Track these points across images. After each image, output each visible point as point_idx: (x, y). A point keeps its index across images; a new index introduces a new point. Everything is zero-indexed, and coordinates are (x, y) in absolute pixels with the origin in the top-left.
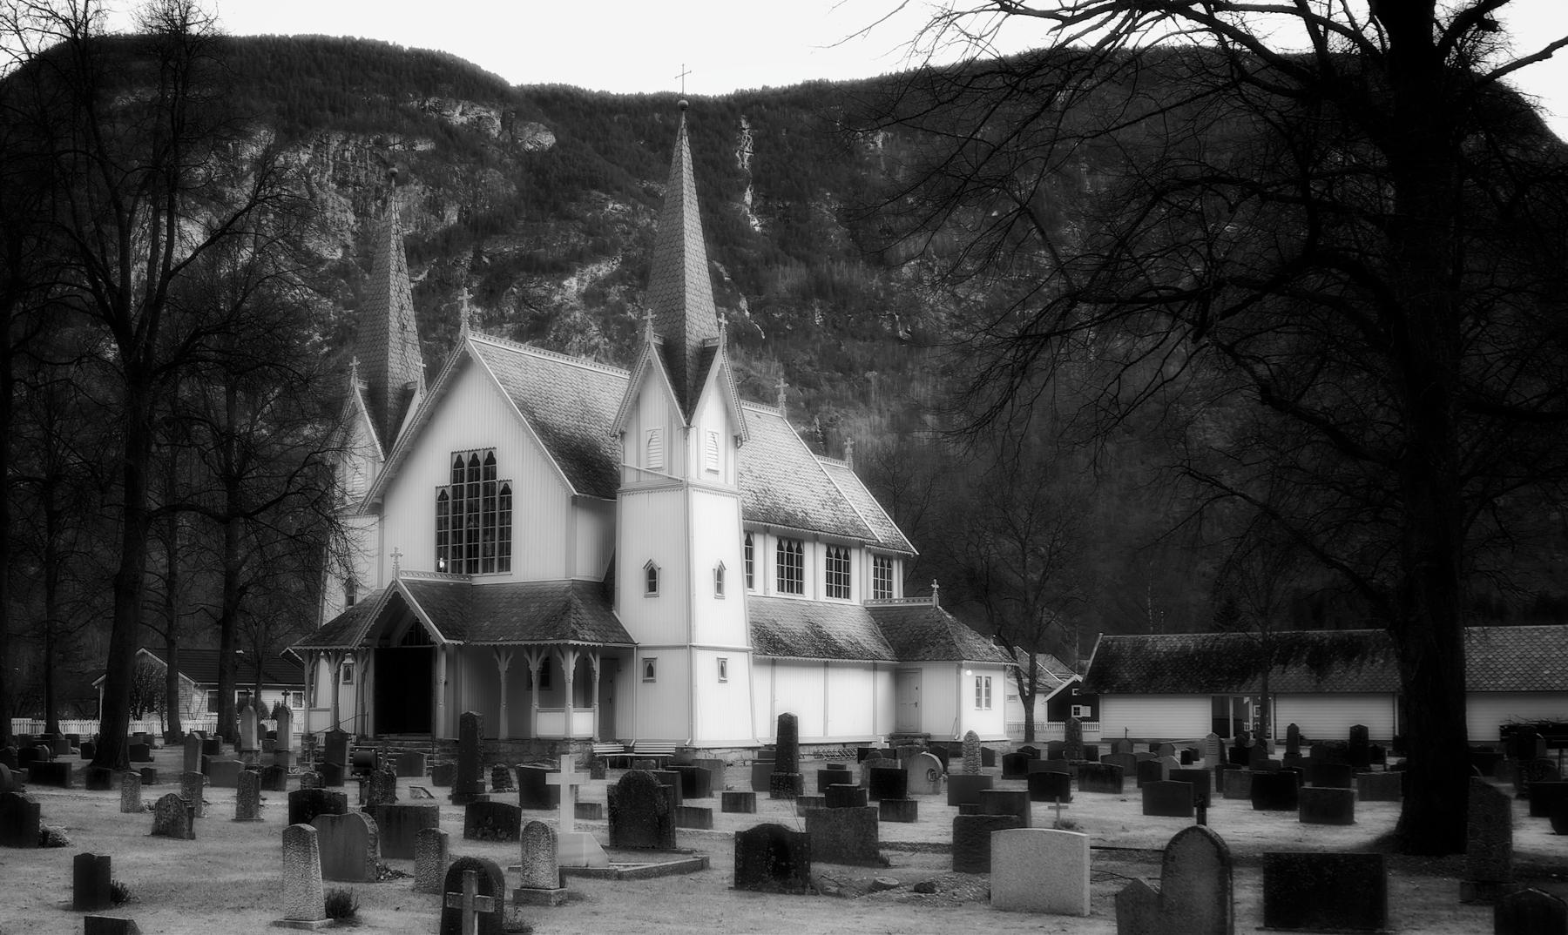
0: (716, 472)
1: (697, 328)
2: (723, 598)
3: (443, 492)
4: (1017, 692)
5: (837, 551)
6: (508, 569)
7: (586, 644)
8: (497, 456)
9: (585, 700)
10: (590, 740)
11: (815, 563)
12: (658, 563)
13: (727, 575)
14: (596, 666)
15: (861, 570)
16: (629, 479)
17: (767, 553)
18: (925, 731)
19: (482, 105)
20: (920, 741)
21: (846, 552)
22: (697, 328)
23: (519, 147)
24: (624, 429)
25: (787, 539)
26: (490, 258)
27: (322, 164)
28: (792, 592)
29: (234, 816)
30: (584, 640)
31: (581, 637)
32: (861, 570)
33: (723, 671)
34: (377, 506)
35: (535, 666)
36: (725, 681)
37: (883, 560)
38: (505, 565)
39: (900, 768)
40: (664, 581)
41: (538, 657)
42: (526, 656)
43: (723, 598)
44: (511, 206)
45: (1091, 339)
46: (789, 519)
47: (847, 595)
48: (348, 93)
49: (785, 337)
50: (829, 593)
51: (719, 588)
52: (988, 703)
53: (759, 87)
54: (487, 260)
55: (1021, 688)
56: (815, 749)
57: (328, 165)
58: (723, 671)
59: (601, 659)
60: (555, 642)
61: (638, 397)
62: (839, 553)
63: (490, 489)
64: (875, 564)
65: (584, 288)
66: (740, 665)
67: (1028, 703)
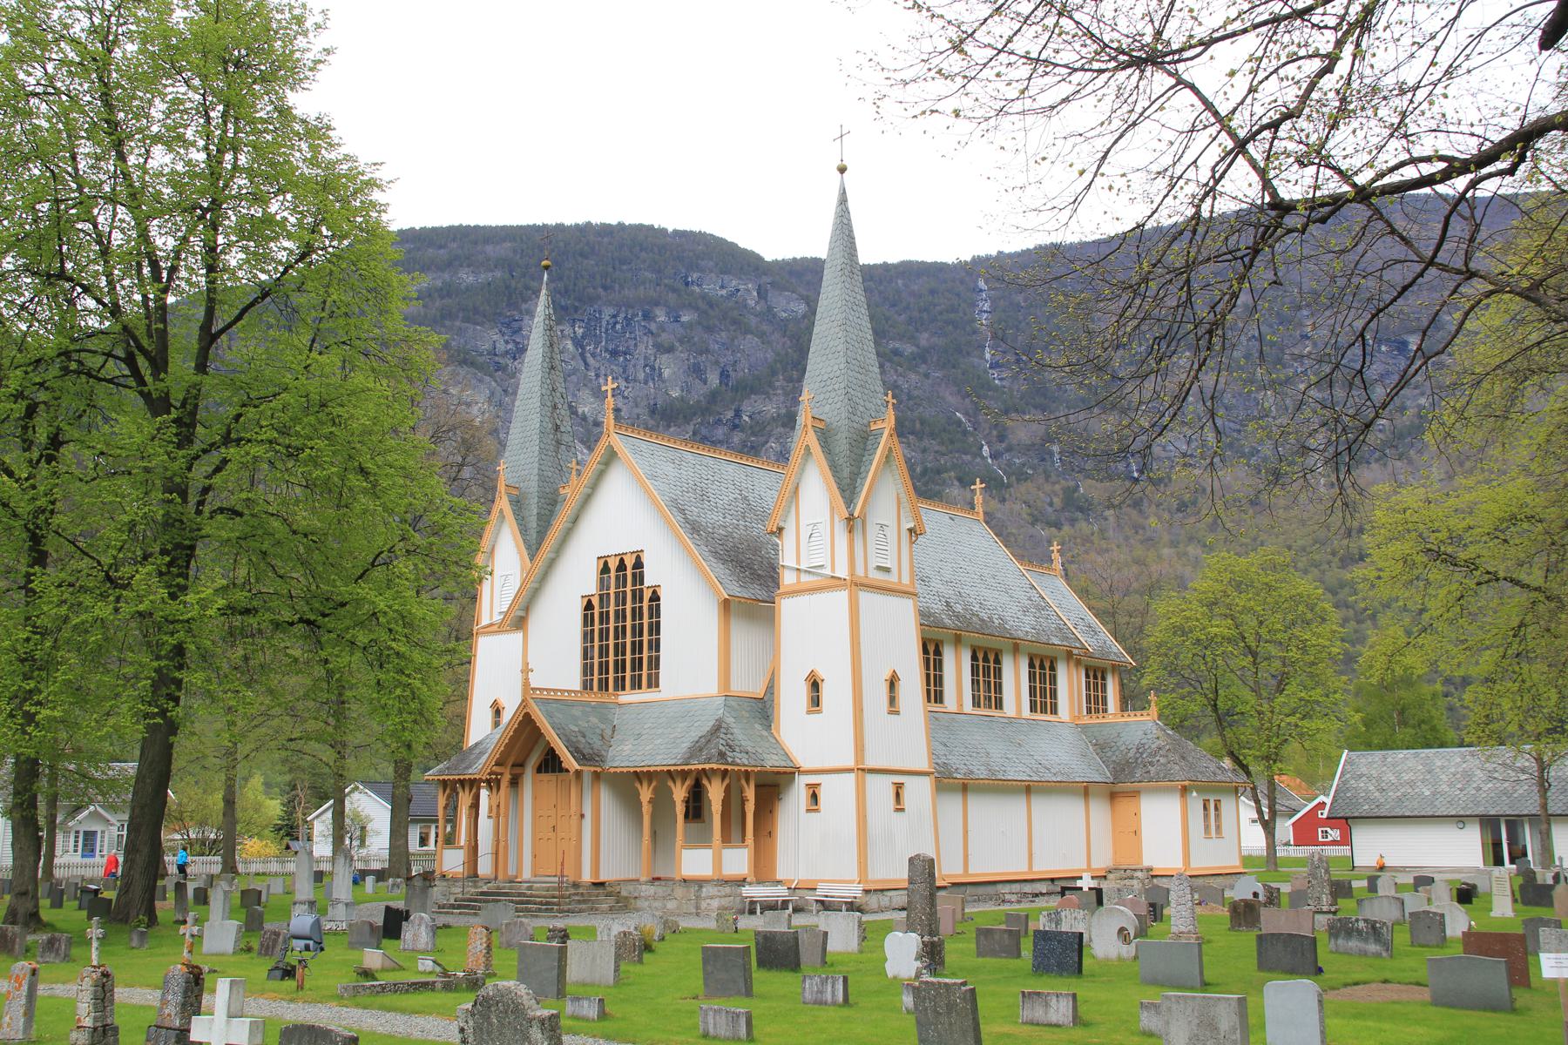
0: (887, 570)
1: (861, 409)
3: (589, 602)
4: (1256, 816)
5: (1042, 662)
6: (657, 686)
7: (736, 768)
8: (645, 560)
10: (742, 882)
11: (1015, 678)
12: (822, 673)
14: (750, 793)
15: (1069, 684)
16: (788, 579)
17: (957, 669)
18: (1146, 863)
19: (740, 279)
20: (1139, 874)
21: (1052, 662)
22: (861, 409)
23: (774, 316)
24: (782, 524)
26: (750, 417)
27: (595, 335)
28: (990, 707)
30: (733, 763)
31: (730, 760)
32: (1069, 684)
34: (518, 620)
35: (680, 793)
36: (817, 811)
37: (1096, 674)
38: (654, 682)
40: (803, 691)
42: (743, 782)
43: (897, 713)
45: (1348, 23)
46: (984, 627)
47: (1054, 711)
48: (617, 273)
49: (1026, 480)
50: (1033, 709)
51: (892, 700)
54: (747, 419)
55: (1260, 812)
56: (1015, 888)
57: (601, 337)
59: (757, 786)
60: (700, 767)
61: (797, 488)
62: (1042, 668)
63: (638, 596)
64: (1087, 676)
66: (919, 791)
67: (1268, 827)
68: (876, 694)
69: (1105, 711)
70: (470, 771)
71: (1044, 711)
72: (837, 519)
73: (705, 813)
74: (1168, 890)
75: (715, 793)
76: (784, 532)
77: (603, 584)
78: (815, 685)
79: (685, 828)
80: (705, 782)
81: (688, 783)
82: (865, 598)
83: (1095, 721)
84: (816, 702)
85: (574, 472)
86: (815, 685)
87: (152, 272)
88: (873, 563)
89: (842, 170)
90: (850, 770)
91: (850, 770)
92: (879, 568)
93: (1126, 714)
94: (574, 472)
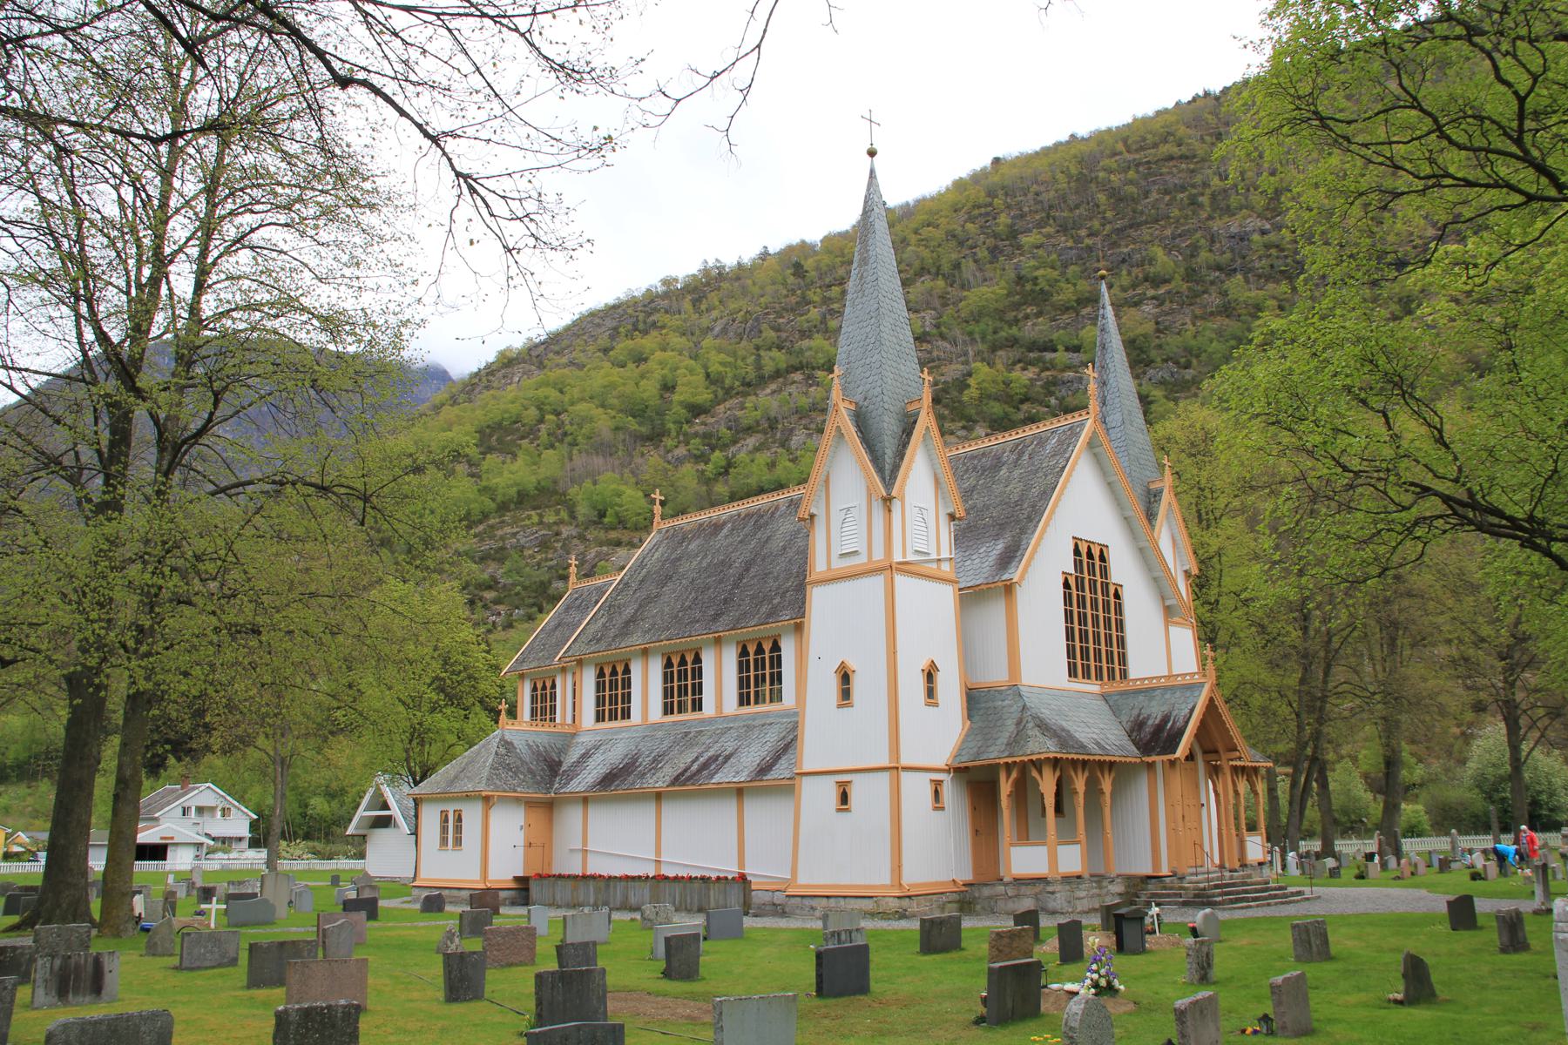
2: (936, 705)
9: (1067, 837)
12: (852, 664)
13: (941, 679)
29: (245, 983)
33: (844, 798)
36: (847, 810)
40: (833, 685)
42: (1035, 774)
43: (936, 705)
44: (1317, 186)
51: (931, 693)
52: (458, 841)
53: (1128, 120)
58: (844, 798)
68: (911, 686)
69: (553, 720)
70: (769, 777)
71: (614, 717)
72: (875, 504)
75: (1047, 784)
76: (816, 519)
77: (1078, 565)
78: (845, 677)
79: (1057, 824)
81: (1014, 775)
82: (900, 579)
83: (539, 729)
84: (846, 694)
86: (845, 677)
87: (168, 198)
89: (872, 153)
90: (906, 769)
91: (906, 769)
92: (842, 555)
93: (534, 723)
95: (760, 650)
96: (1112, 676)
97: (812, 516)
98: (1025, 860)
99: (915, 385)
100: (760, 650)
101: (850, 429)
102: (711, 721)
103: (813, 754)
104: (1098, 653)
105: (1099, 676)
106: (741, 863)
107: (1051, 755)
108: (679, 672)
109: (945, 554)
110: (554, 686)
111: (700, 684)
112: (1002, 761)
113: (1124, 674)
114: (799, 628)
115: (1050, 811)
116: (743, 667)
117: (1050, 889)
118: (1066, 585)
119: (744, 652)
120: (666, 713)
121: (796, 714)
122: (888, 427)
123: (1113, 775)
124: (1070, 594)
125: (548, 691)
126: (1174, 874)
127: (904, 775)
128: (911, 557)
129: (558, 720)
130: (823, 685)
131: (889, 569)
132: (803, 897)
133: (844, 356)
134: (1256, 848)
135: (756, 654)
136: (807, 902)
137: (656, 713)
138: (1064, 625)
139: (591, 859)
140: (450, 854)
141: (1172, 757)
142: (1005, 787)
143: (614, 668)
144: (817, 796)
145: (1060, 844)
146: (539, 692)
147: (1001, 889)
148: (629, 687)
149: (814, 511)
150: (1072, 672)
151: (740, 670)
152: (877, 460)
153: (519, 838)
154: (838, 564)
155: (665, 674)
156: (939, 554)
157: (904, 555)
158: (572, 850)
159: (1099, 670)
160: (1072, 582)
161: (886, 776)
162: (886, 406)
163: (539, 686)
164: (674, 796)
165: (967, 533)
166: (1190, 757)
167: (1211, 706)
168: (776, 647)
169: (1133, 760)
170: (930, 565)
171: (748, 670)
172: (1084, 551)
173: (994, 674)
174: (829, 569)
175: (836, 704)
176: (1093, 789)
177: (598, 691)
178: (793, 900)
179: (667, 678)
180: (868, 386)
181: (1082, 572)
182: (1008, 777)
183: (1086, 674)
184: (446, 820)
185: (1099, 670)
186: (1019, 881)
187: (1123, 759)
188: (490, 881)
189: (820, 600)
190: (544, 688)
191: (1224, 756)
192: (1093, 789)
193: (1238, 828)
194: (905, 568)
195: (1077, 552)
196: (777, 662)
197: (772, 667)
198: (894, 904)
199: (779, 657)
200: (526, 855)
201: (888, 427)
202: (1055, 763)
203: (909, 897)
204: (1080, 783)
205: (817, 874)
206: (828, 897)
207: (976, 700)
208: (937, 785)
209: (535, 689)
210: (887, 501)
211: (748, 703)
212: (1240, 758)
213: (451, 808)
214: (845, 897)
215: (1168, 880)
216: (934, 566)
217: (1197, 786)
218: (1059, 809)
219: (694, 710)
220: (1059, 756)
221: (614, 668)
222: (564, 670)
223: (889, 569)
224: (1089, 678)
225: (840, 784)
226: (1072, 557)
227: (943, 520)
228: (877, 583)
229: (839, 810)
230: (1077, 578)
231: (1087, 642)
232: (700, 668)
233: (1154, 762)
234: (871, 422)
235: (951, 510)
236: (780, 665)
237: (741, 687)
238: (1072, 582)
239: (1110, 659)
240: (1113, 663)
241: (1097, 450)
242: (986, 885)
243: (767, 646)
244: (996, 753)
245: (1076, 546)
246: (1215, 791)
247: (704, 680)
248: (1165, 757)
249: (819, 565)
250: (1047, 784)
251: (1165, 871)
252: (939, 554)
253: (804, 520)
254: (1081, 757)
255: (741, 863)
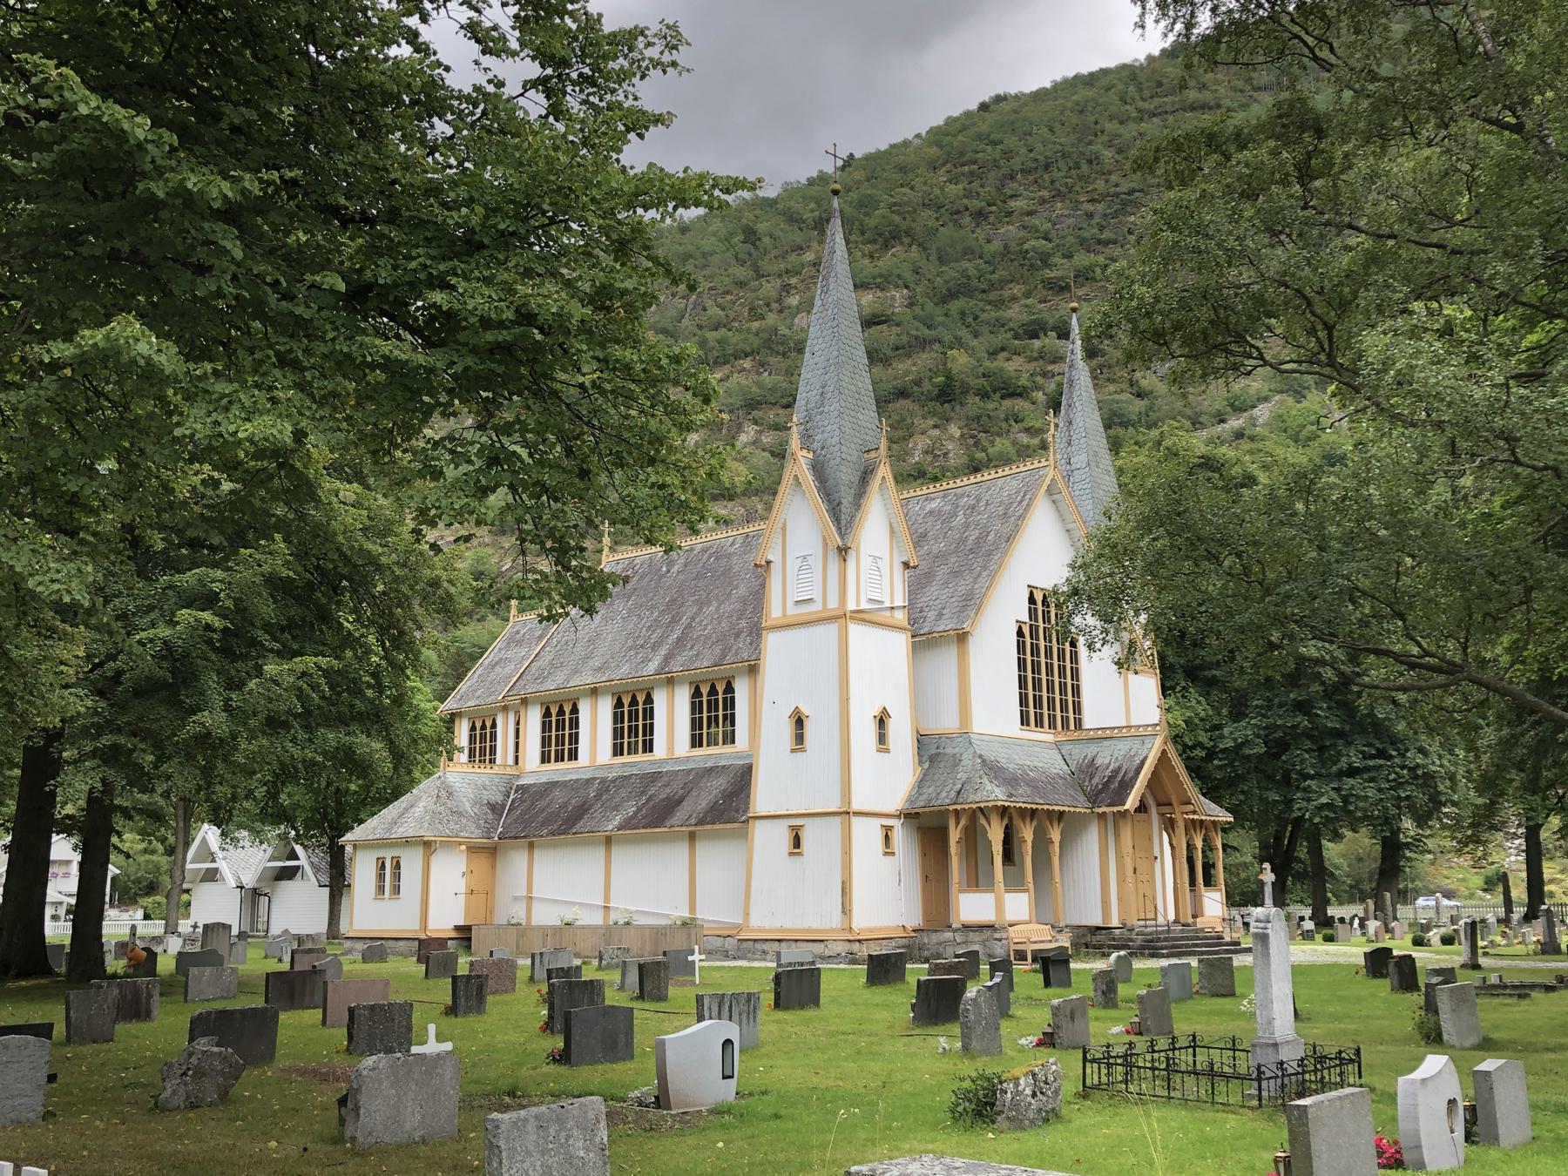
2: (887, 751)
9: (1015, 884)
12: (805, 710)
13: (892, 726)
25: (555, 702)
33: (797, 842)
36: (799, 854)
39: (908, 966)
40: (787, 730)
41: (957, 824)
42: (983, 821)
43: (887, 751)
51: (882, 738)
52: (396, 890)
58: (797, 842)
65: (321, 494)
68: (863, 732)
69: (492, 761)
73: (1016, 857)
74: (1262, 905)
77: (1032, 613)
78: (799, 722)
80: (983, 821)
81: (963, 822)
82: (855, 630)
84: (800, 738)
85: (1052, 425)
86: (799, 722)
88: (793, 596)
90: (857, 814)
91: (857, 814)
92: (797, 602)
94: (1052, 425)
95: (713, 691)
96: (1053, 725)
97: (768, 563)
98: (972, 907)
99: (872, 433)
100: (713, 691)
101: (808, 478)
102: (662, 762)
103: (763, 798)
104: (1051, 701)
105: (1053, 725)
106: (692, 908)
107: (999, 803)
108: (630, 712)
109: (899, 602)
110: (494, 725)
111: (652, 725)
112: (951, 808)
113: (1079, 724)
114: (753, 670)
115: (998, 860)
116: (696, 707)
117: (997, 936)
118: (1020, 633)
119: (697, 693)
120: (615, 754)
121: (750, 756)
122: (845, 476)
123: (1062, 825)
124: (1024, 642)
125: (488, 731)
126: (1124, 926)
127: (855, 821)
128: (864, 606)
129: (498, 762)
130: (777, 730)
131: (840, 617)
132: (755, 940)
133: (804, 402)
134: (1214, 904)
135: (709, 695)
136: (758, 946)
137: (605, 754)
138: (1017, 673)
139: (535, 906)
140: (387, 904)
141: (1121, 808)
142: (955, 835)
143: (561, 707)
144: (769, 840)
145: (1007, 891)
146: (478, 732)
147: (948, 935)
148: (577, 727)
149: (770, 557)
150: (1024, 720)
151: (693, 712)
152: (835, 511)
153: (461, 885)
154: (792, 610)
155: (615, 714)
156: (892, 602)
157: (858, 603)
158: (515, 898)
159: (1065, 721)
160: (1026, 630)
161: (838, 819)
162: (844, 456)
163: (478, 725)
164: (627, 841)
165: (918, 577)
166: (1142, 808)
167: (1163, 758)
168: (729, 689)
169: (1083, 810)
170: (883, 613)
171: (701, 712)
172: (1039, 597)
173: (947, 722)
174: (784, 615)
175: (789, 749)
176: (1041, 842)
177: (544, 731)
178: (745, 945)
179: (618, 718)
180: (826, 435)
181: (1036, 621)
182: (957, 824)
183: (1039, 723)
184: (383, 867)
185: (1065, 721)
186: (967, 927)
187: (1072, 809)
188: (431, 931)
189: (775, 646)
190: (483, 727)
191: (1178, 809)
192: (1041, 842)
193: (1193, 882)
194: (860, 617)
195: (1032, 600)
196: (730, 703)
197: (725, 709)
198: (841, 948)
199: (733, 699)
200: (467, 902)
201: (845, 476)
202: (1003, 812)
203: (859, 941)
204: (1027, 833)
205: (765, 919)
206: (779, 941)
207: (930, 750)
208: (888, 831)
209: (473, 728)
210: (843, 551)
211: (701, 745)
212: (1194, 812)
213: (388, 855)
214: (796, 941)
215: (1117, 931)
216: (888, 614)
217: (1150, 839)
218: (1008, 857)
219: (644, 751)
220: (1006, 804)
221: (561, 707)
222: (505, 709)
223: (840, 617)
224: (1042, 726)
225: (792, 828)
226: (1027, 605)
227: (898, 568)
228: (831, 630)
229: (791, 854)
230: (1031, 626)
231: (1040, 691)
232: (652, 709)
233: (1104, 813)
234: (827, 472)
235: (905, 559)
236: (652, 717)
237: (693, 728)
238: (1026, 630)
239: (1064, 708)
240: (1067, 712)
241: (1055, 497)
242: (936, 931)
243: (720, 688)
244: (945, 798)
245: (1031, 594)
246: (1171, 845)
247: (737, 711)
248: (1115, 809)
249: (775, 609)
250: (996, 834)
251: (1115, 922)
252: (892, 602)
253: (761, 566)
254: (1029, 806)
255: (692, 908)
